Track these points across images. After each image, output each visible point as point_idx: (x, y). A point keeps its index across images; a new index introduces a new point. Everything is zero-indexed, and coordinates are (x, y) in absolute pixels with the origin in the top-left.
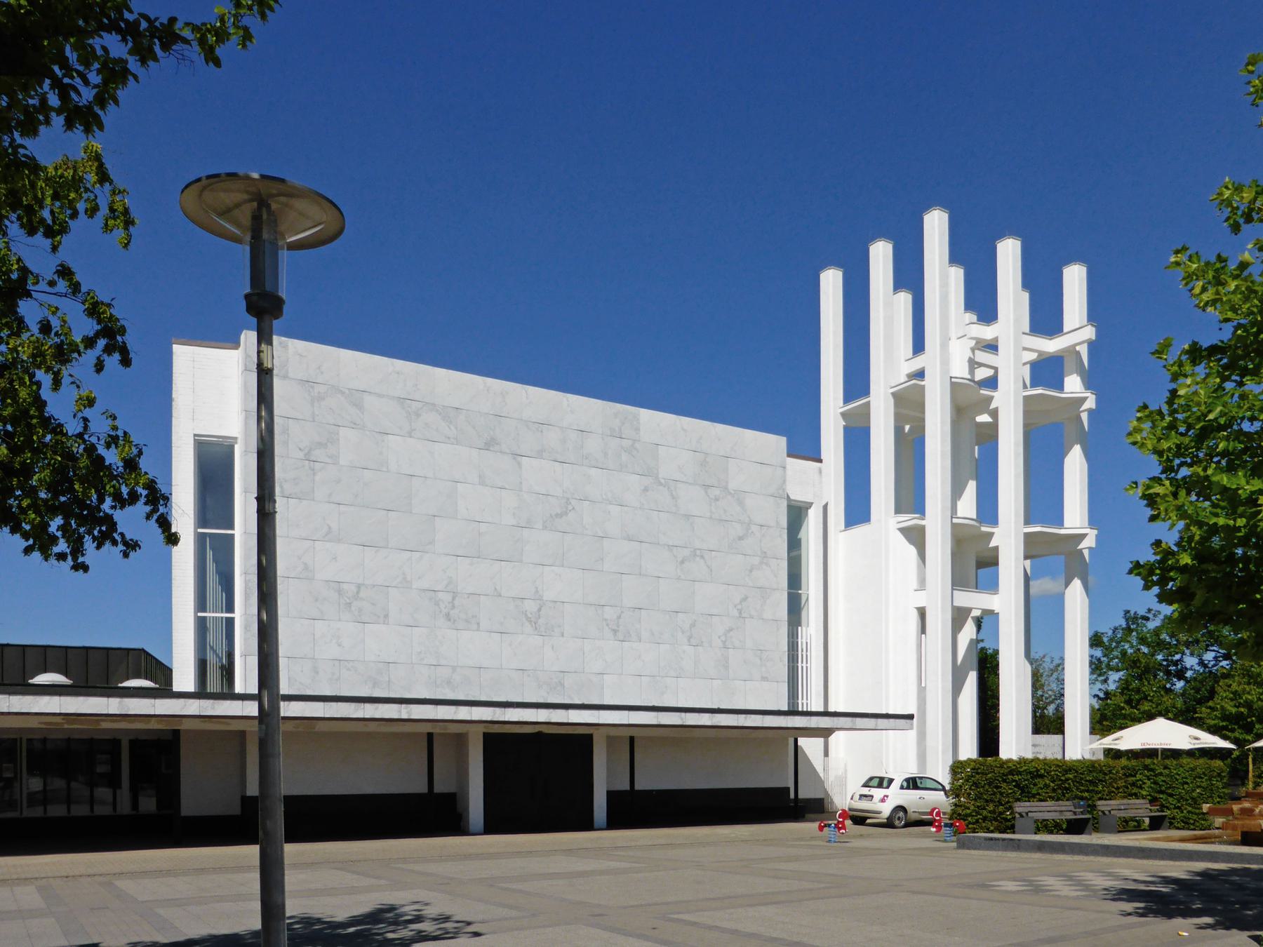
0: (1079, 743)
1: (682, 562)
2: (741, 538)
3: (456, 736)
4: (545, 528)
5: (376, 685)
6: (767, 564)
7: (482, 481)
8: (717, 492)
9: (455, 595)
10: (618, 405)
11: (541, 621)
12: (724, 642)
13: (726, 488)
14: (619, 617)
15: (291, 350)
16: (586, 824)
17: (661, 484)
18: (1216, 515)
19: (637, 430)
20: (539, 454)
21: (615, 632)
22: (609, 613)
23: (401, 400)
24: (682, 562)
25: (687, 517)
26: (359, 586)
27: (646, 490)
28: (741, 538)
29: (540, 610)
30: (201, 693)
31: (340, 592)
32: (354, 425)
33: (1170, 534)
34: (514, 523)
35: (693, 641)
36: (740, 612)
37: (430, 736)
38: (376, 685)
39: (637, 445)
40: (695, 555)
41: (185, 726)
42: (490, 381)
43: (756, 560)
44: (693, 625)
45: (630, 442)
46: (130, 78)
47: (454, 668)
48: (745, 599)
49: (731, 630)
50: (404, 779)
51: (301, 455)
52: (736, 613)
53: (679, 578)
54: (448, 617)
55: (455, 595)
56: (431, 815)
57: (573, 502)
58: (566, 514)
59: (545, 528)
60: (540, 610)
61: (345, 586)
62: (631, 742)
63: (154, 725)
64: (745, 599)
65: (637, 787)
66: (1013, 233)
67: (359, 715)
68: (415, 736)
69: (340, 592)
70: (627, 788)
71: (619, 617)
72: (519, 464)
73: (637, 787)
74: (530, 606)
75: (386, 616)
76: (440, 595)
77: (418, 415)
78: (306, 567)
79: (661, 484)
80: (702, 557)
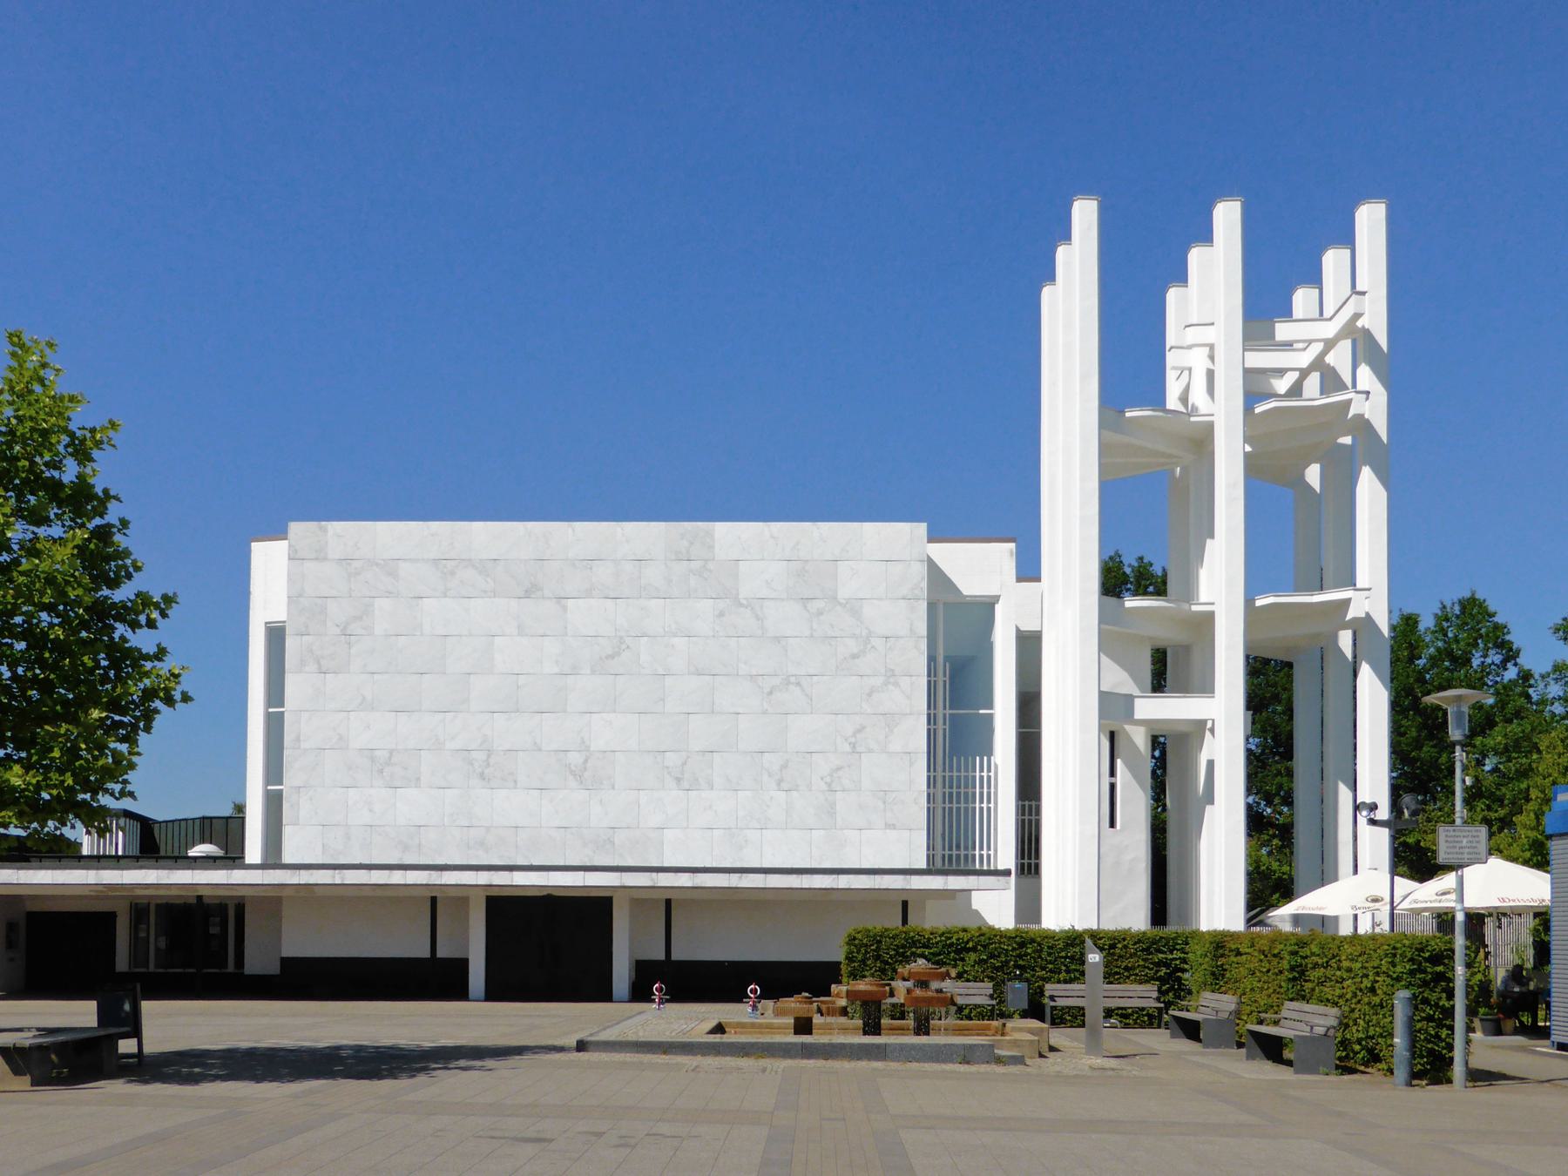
0: (1358, 891)
1: (771, 693)
2: (854, 656)
3: (460, 897)
4: (593, 672)
5: (406, 848)
6: (896, 684)
7: (521, 631)
8: (820, 604)
9: (490, 752)
10: (686, 524)
11: (586, 774)
12: (829, 785)
13: (835, 598)
14: (684, 763)
15: (330, 533)
16: (602, 993)
17: (741, 605)
18: (38, 519)
19: (711, 547)
20: (588, 594)
21: (678, 780)
22: (672, 759)
23: (435, 560)
24: (771, 693)
25: (777, 639)
26: (391, 752)
27: (721, 614)
28: (854, 656)
29: (586, 761)
30: (262, 867)
31: (373, 760)
32: (389, 594)
33: (1128, 570)
34: (556, 670)
35: (785, 786)
36: (853, 746)
37: (668, 902)
38: (406, 848)
39: (711, 566)
40: (789, 683)
41: (285, 893)
42: (531, 525)
43: (879, 681)
44: (784, 766)
45: (699, 563)
46: (1359, 324)
47: (488, 829)
48: (861, 729)
49: (839, 769)
50: (405, 942)
51: (338, 631)
52: (848, 748)
53: (765, 712)
54: (482, 776)
55: (490, 752)
56: (437, 979)
57: (628, 641)
58: (619, 654)
59: (593, 672)
60: (586, 761)
61: (377, 753)
62: (668, 906)
63: (174, 892)
64: (861, 729)
65: (440, 954)
66: (1086, 192)
67: (295, 881)
68: (657, 901)
69: (373, 760)
70: (662, 957)
71: (684, 763)
72: (565, 608)
73: (440, 954)
74: (575, 758)
75: (418, 779)
76: (474, 755)
77: (453, 573)
78: (341, 738)
79: (741, 605)
80: (798, 684)
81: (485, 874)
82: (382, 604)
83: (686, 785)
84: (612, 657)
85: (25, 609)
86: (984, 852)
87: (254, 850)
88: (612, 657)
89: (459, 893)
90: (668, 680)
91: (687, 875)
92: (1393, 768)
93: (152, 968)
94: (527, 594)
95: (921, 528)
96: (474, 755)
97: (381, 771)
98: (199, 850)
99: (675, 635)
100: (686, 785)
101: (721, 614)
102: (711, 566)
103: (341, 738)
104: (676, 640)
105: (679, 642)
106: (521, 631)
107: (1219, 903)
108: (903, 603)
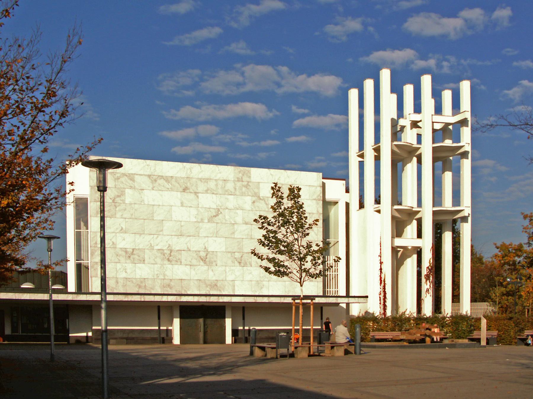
4: (209, 222)
5: (140, 287)
9: (171, 251)
14: (242, 257)
17: (261, 199)
19: (250, 177)
20: (207, 191)
21: (240, 263)
26: (133, 250)
27: (254, 202)
29: (207, 255)
31: (126, 252)
34: (196, 220)
37: (244, 308)
39: (250, 184)
45: (246, 183)
47: (171, 280)
54: (169, 260)
59: (209, 222)
60: (207, 255)
61: (128, 250)
67: (126, 299)
69: (126, 252)
71: (242, 257)
72: (198, 197)
75: (144, 260)
77: (156, 181)
78: (113, 243)
79: (261, 199)
81: (158, 297)
82: (128, 191)
83: (242, 265)
84: (215, 216)
85: (296, 192)
86: (329, 290)
87: (72, 286)
88: (215, 216)
89: (222, 305)
90: (236, 226)
91: (362, 299)
92: (471, 264)
93: (21, 334)
94: (185, 190)
95: (321, 174)
96: (165, 251)
97: (129, 257)
98: (26, 286)
99: (238, 209)
100: (242, 265)
101: (254, 202)
102: (250, 184)
103: (113, 243)
104: (237, 211)
105: (239, 212)
106: (182, 205)
107: (428, 310)
108: (314, 201)
